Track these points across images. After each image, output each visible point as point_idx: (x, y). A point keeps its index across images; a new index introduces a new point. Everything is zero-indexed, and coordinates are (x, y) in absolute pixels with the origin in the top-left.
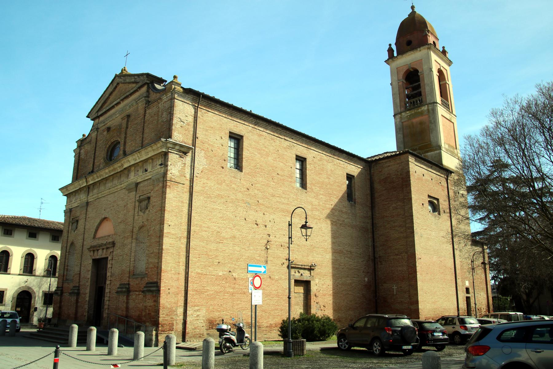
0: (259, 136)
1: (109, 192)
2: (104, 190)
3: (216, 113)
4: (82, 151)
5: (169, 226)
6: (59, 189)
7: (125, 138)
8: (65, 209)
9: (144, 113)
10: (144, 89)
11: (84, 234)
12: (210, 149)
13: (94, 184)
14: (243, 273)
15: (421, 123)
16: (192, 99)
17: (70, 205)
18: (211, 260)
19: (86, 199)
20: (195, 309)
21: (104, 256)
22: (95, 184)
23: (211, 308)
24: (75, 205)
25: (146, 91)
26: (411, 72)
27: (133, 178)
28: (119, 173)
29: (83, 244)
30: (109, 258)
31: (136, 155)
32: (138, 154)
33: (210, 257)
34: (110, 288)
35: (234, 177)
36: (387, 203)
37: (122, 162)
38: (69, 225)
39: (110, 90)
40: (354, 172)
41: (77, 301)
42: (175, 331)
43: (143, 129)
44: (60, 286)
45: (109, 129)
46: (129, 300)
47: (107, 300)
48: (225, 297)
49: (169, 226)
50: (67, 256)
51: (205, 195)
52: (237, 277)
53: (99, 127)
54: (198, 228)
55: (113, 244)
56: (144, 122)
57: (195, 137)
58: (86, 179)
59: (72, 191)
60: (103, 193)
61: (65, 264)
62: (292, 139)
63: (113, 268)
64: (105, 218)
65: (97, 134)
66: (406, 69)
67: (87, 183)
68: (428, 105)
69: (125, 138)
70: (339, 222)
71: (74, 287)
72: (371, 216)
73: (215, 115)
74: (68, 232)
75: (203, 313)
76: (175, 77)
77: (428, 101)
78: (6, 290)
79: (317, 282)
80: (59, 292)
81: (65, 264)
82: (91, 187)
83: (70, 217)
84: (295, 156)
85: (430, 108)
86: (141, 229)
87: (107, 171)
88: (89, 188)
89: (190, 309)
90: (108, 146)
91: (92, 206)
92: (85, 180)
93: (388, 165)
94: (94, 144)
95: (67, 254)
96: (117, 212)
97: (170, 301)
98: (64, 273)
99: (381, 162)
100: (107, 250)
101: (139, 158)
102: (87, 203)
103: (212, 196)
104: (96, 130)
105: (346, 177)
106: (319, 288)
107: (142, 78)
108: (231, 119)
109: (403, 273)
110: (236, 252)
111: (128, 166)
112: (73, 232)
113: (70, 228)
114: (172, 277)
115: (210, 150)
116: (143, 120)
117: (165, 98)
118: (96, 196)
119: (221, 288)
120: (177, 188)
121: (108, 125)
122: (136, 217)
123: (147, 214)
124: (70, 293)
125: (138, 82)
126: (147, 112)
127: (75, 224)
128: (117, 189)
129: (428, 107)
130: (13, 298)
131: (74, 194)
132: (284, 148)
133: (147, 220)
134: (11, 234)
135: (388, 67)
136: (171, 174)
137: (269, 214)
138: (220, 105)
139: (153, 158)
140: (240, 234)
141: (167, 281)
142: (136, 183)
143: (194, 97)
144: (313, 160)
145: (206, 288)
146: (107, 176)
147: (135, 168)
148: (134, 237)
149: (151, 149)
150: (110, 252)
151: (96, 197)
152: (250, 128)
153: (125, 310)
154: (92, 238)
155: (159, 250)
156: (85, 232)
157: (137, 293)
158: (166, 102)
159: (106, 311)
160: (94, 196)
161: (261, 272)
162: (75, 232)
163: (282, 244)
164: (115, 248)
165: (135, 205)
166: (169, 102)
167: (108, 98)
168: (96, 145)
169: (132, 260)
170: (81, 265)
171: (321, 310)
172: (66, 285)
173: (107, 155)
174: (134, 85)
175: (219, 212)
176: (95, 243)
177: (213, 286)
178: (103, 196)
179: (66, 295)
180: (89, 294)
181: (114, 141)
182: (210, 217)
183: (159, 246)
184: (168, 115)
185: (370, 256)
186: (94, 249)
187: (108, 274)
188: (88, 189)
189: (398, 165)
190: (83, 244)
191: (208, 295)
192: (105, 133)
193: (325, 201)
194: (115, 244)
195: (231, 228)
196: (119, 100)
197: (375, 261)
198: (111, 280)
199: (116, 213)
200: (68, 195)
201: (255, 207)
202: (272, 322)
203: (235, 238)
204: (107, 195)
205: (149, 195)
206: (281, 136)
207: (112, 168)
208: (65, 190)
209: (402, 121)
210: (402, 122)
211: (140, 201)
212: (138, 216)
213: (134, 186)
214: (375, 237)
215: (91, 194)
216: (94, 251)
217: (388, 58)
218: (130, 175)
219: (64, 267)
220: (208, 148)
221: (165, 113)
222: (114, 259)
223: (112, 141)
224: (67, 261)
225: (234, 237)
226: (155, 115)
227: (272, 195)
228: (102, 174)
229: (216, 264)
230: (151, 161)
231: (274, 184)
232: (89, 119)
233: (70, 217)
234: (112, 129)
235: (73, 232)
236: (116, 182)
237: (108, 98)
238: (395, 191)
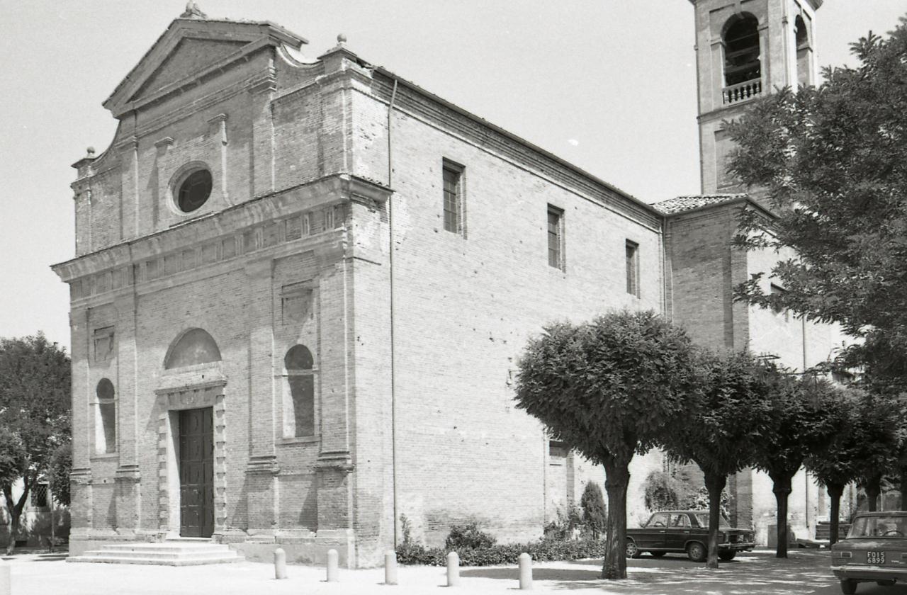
3: (420, 118)
16: (381, 88)
26: (739, 20)
39: (166, 50)
40: (638, 236)
57: (391, 170)
62: (542, 171)
67: (132, 257)
75: (419, 503)
76: (340, 39)
89: (401, 496)
93: (703, 223)
108: (444, 132)
115: (414, 196)
138: (427, 101)
143: (385, 84)
145: (422, 458)
165: (273, 303)
189: (723, 225)
193: (594, 294)
206: (524, 167)
212: (283, 325)
225: (460, 364)
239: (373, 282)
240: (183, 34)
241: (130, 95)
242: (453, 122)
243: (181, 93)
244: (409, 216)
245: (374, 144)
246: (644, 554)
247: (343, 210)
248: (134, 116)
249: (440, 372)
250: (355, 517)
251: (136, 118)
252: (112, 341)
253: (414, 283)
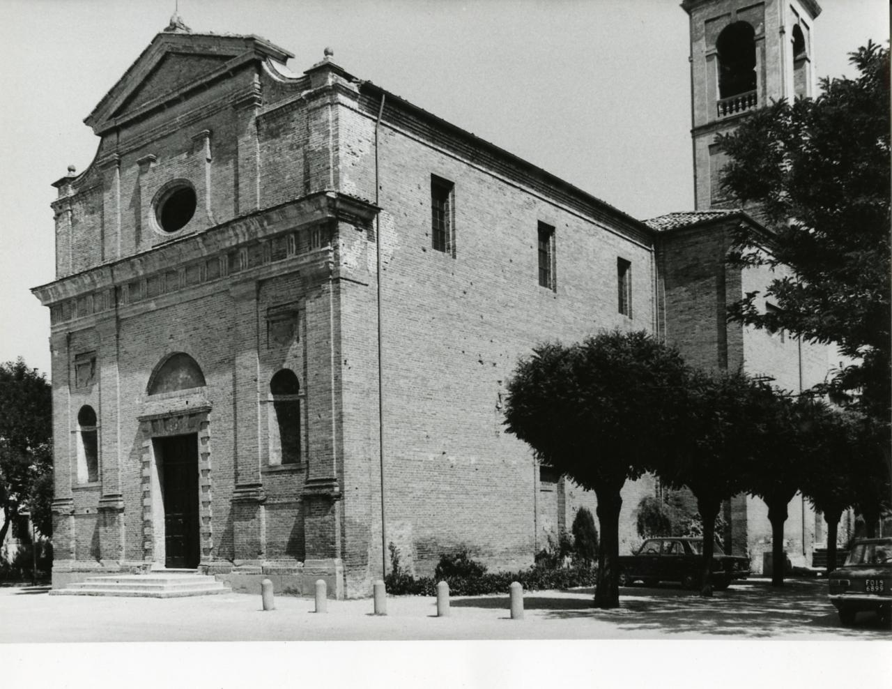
0: (479, 183)
3: (408, 134)
12: (402, 211)
18: (415, 432)
33: (414, 427)
39: (149, 66)
48: (439, 501)
51: (399, 306)
52: (455, 463)
54: (393, 372)
67: (113, 279)
73: (407, 138)
75: (407, 531)
76: (327, 53)
96: (208, 341)
103: (412, 307)
132: (521, 207)
136: (345, 265)
137: (500, 341)
145: (410, 485)
152: (464, 166)
193: (585, 314)
202: (508, 545)
212: (268, 348)
231: (506, 281)
238: (707, 294)
240: (166, 48)
241: (112, 111)
244: (397, 234)
245: (361, 160)
247: (328, 231)
250: (343, 547)
252: (93, 367)
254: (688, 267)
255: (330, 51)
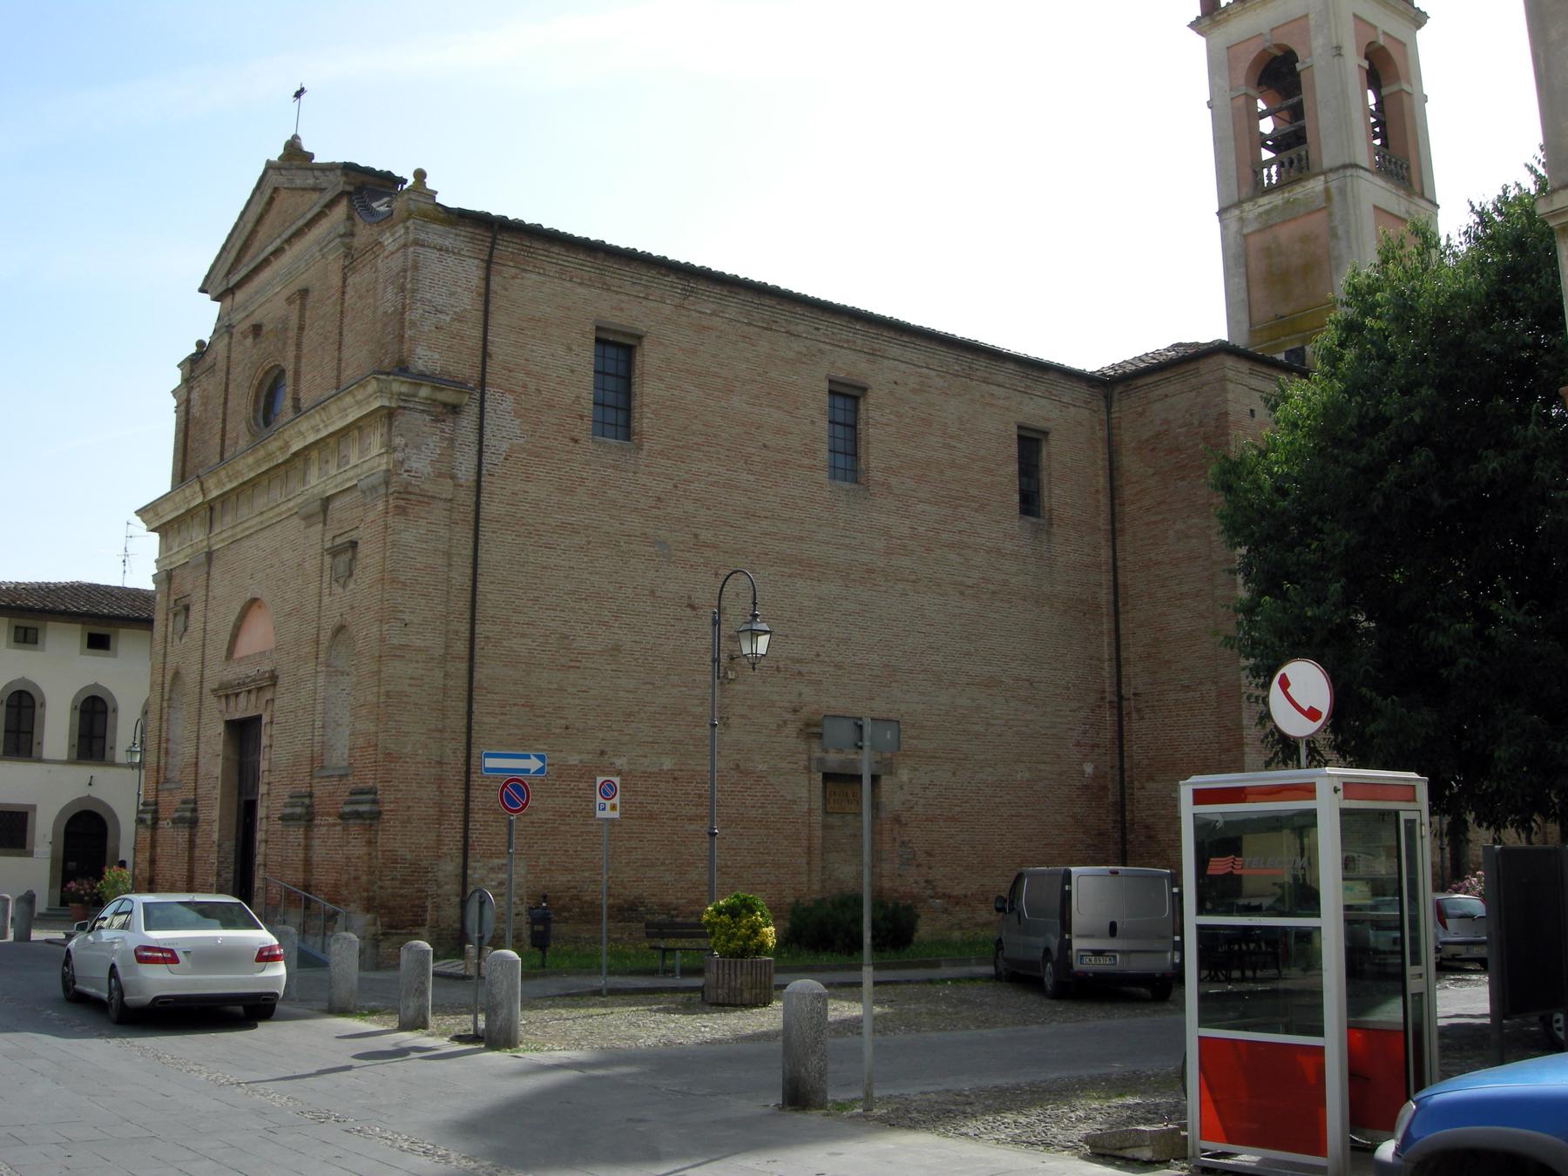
1: (261, 522)
2: (248, 516)
4: (195, 395)
5: (406, 625)
6: (136, 512)
7: (298, 358)
8: (156, 571)
9: (340, 283)
10: (341, 210)
11: (204, 645)
12: (532, 387)
13: (224, 497)
14: (646, 757)
15: (1305, 239)
17: (167, 561)
18: (540, 720)
19: (205, 543)
20: (490, 865)
21: (251, 713)
22: (226, 497)
23: (543, 860)
24: (180, 559)
25: (345, 216)
27: (319, 481)
28: (283, 467)
29: (202, 676)
30: (265, 719)
31: (317, 416)
32: (323, 414)
34: (268, 807)
35: (615, 467)
36: (1160, 517)
37: (286, 436)
38: (167, 620)
39: (257, 209)
41: (192, 844)
42: (431, 927)
43: (341, 334)
44: (151, 800)
45: (257, 330)
46: (312, 838)
47: (262, 841)
49: (406, 625)
50: (165, 711)
53: (234, 322)
55: (273, 679)
56: (342, 312)
58: (202, 484)
59: (169, 518)
60: (246, 525)
61: (160, 736)
63: (273, 749)
64: (254, 601)
65: (230, 344)
66: (1258, 51)
67: (204, 495)
68: (1324, 173)
69: (298, 358)
70: (989, 586)
71: (184, 802)
72: (1111, 561)
74: (166, 642)
77: (1327, 162)
78: (34, 808)
79: (905, 778)
80: (148, 817)
81: (160, 736)
82: (218, 506)
83: (169, 595)
84: (825, 385)
85: (1333, 185)
86: (340, 635)
87: (251, 460)
88: (212, 509)
90: (256, 382)
91: (302, 527)
92: (197, 487)
94: (223, 374)
95: (165, 704)
96: (280, 583)
97: (413, 843)
98: (158, 763)
99: (1141, 382)
100: (260, 694)
101: (326, 426)
102: (210, 555)
104: (227, 332)
105: (1015, 437)
106: (910, 797)
107: (331, 176)
109: (1205, 746)
110: (622, 694)
111: (300, 447)
112: (177, 640)
113: (170, 629)
114: (418, 775)
116: (339, 308)
117: (390, 240)
118: (230, 533)
119: (575, 801)
120: (428, 512)
121: (254, 320)
122: (326, 600)
123: (352, 590)
124: (174, 821)
125: (325, 189)
126: (350, 281)
127: (181, 618)
128: (280, 514)
129: (1326, 182)
130: (55, 834)
131: (176, 526)
133: (352, 608)
134: (35, 642)
135: (1199, 44)
136: (406, 474)
139: (360, 424)
140: (637, 638)
141: (402, 787)
142: (321, 499)
143: (478, 231)
144: (891, 393)
146: (252, 475)
147: (320, 453)
148: (322, 657)
149: (352, 400)
150: (267, 701)
151: (229, 537)
153: (301, 868)
154: (224, 659)
155: (379, 697)
156: (207, 642)
157: (330, 819)
158: (392, 253)
159: (261, 872)
160: (224, 535)
161: (528, 771)
162: (183, 641)
163: (781, 665)
164: (277, 687)
165: (322, 563)
166: (400, 254)
167: (253, 232)
168: (227, 378)
169: (318, 724)
170: (198, 738)
171: (918, 866)
172: (164, 797)
173: (256, 411)
174: (315, 196)
175: (566, 577)
176: (234, 672)
177: (548, 797)
178: (247, 533)
179: (165, 824)
180: (220, 823)
181: (272, 368)
182: (536, 594)
183: (379, 686)
184: (397, 294)
185: (1104, 692)
186: (227, 692)
187: (264, 765)
188: (211, 510)
189: (1194, 393)
190: (202, 676)
191: (532, 823)
192: (249, 341)
194: (277, 677)
195: (605, 624)
196: (278, 242)
197: (1120, 709)
198: (269, 784)
199: (279, 587)
200: (163, 530)
201: (687, 554)
203: (619, 650)
204: (256, 532)
205: (354, 535)
207: (262, 453)
208: (151, 514)
209: (1245, 231)
210: (1245, 236)
211: (335, 552)
212: (330, 595)
213: (316, 506)
214: (1122, 632)
215: (217, 530)
216: (227, 697)
217: (1199, 14)
218: (308, 472)
219: (159, 743)
220: (525, 386)
221: (390, 288)
222: (275, 720)
223: (267, 368)
224: (164, 725)
225: (617, 649)
226: (368, 291)
227: (747, 513)
228: (240, 468)
229: (557, 731)
230: (356, 432)
231: (752, 478)
232: (207, 297)
233: (169, 595)
234: (265, 329)
235: (178, 641)
236: (277, 494)
237: (253, 232)
238: (1183, 478)
239: (433, 527)
242: (618, 271)
243: (272, 262)
244: (518, 421)
245: (453, 320)
246: (113, 980)
248: (231, 296)
249: (572, 664)
251: (233, 298)
253: (523, 524)
254: (1157, 435)
255: (1337, 58)
